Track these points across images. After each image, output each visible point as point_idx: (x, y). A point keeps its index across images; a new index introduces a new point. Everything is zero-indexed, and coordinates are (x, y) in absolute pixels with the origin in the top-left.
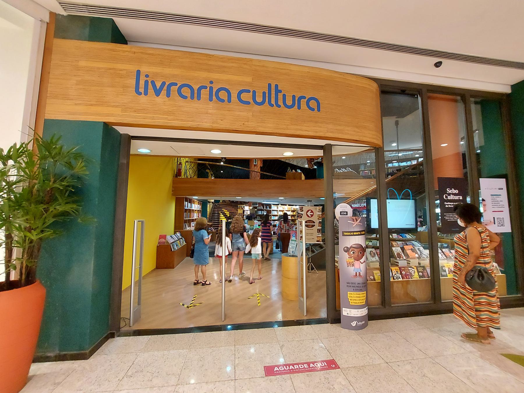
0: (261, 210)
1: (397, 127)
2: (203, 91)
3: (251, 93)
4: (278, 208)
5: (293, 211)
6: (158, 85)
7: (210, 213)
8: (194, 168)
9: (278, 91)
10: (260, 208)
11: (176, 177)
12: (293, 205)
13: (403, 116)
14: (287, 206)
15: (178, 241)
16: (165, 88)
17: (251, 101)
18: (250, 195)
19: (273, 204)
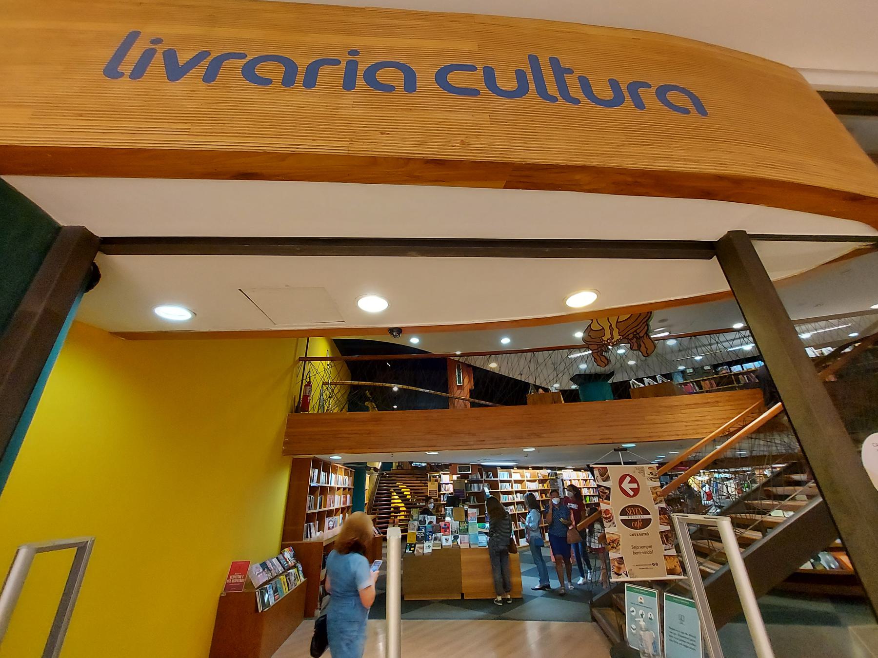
0: (478, 482)
2: (324, 70)
3: (480, 72)
4: (510, 476)
5: (542, 482)
6: (184, 57)
7: (372, 494)
8: (339, 395)
9: (560, 72)
10: (474, 477)
11: (297, 411)
12: (541, 468)
14: (531, 471)
15: (283, 577)
16: (206, 63)
17: (482, 87)
18: (456, 447)
19: (503, 467)
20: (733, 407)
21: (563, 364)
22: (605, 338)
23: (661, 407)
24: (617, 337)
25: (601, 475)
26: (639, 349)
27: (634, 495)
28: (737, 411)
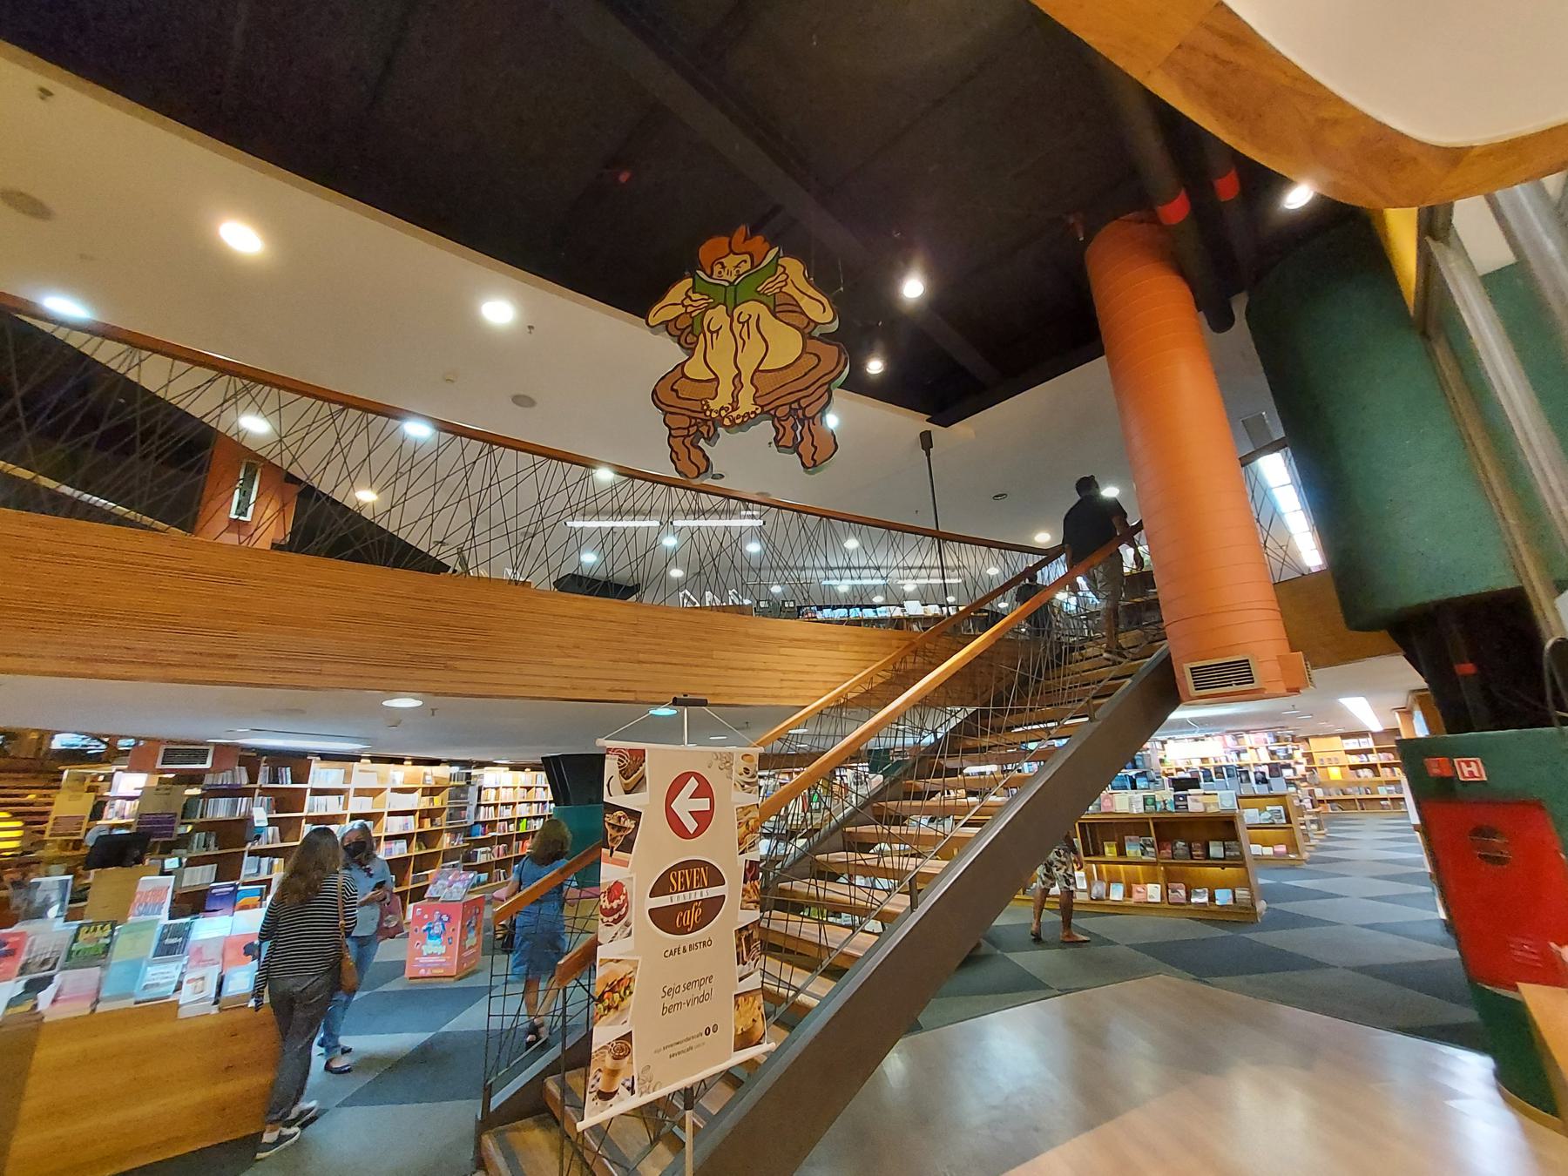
0: (234, 792)
1: (928, 454)
4: (348, 776)
5: (431, 792)
10: (224, 779)
12: (436, 762)
13: (946, 424)
19: (325, 757)
20: (861, 656)
21: (563, 496)
22: (715, 405)
23: (747, 635)
24: (746, 405)
25: (624, 773)
26: (795, 448)
27: (698, 832)
28: (862, 664)
